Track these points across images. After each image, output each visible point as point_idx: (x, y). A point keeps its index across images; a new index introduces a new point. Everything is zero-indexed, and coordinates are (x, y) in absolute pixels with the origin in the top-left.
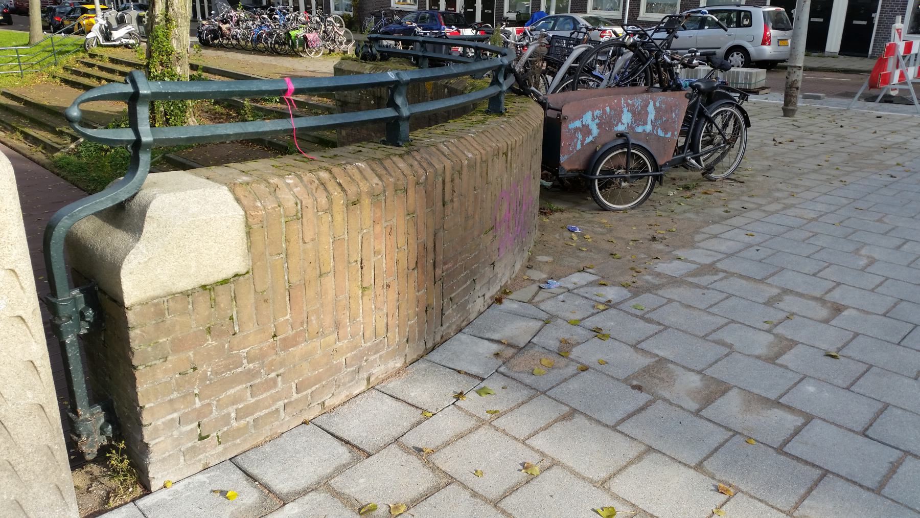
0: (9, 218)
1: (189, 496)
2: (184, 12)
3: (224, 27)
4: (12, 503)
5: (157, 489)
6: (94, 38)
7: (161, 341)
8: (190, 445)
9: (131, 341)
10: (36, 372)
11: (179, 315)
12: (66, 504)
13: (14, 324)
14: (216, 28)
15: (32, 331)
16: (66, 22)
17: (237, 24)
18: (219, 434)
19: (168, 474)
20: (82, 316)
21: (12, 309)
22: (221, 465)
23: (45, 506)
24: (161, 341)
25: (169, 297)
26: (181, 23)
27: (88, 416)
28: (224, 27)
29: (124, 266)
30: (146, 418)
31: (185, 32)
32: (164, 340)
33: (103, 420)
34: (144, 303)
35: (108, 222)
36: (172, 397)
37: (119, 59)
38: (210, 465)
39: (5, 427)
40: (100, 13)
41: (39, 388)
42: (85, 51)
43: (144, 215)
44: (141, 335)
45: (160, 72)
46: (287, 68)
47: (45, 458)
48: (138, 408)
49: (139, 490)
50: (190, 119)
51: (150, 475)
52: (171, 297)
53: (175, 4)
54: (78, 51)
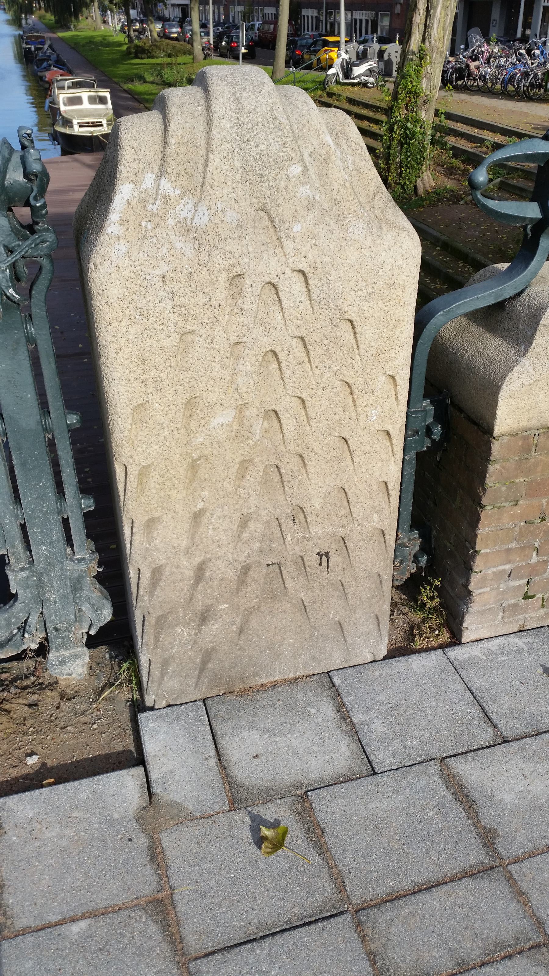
0: (405, 313)
1: (506, 662)
2: (441, 45)
3: (473, 65)
4: (335, 624)
5: (468, 641)
6: (335, 74)
7: (518, 481)
8: (513, 601)
9: (488, 476)
10: (386, 495)
11: (546, 454)
12: (381, 635)
13: (380, 439)
14: (463, 66)
15: (395, 449)
16: (306, 56)
17: (488, 61)
18: (546, 596)
19: (482, 628)
20: (429, 431)
21: (382, 421)
22: (539, 630)
23: (362, 634)
24: (518, 481)
25: (542, 431)
26: (435, 60)
27: (406, 540)
28: (473, 65)
29: (504, 386)
30: (478, 564)
31: (437, 70)
32: (522, 480)
33: (417, 548)
34: (513, 435)
35: (474, 322)
36: (510, 546)
37: (357, 99)
38: (526, 628)
39: (346, 548)
40: (343, 46)
41: (386, 512)
42: (324, 89)
43: (537, 323)
44: (500, 471)
45: (403, 116)
46: (541, 117)
47: (373, 586)
48: (472, 551)
49: (446, 636)
50: (425, 173)
51: (465, 625)
52: (544, 430)
53: (433, 36)
54: (317, 88)
